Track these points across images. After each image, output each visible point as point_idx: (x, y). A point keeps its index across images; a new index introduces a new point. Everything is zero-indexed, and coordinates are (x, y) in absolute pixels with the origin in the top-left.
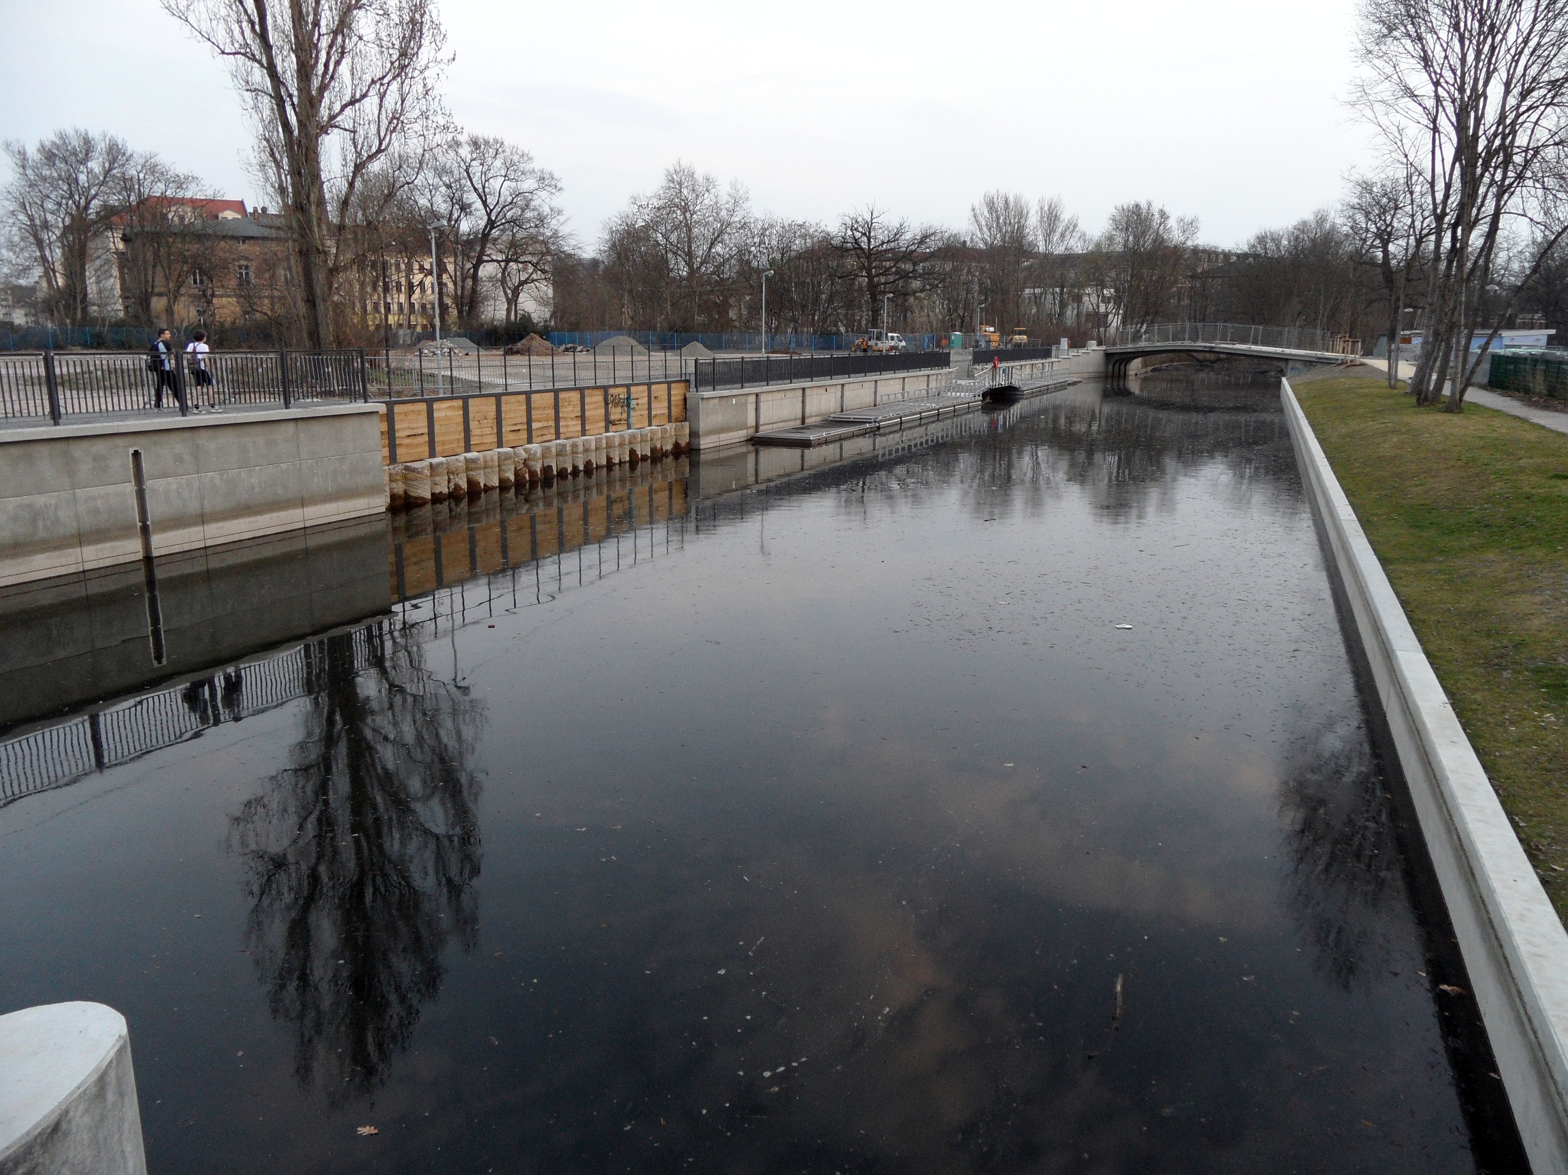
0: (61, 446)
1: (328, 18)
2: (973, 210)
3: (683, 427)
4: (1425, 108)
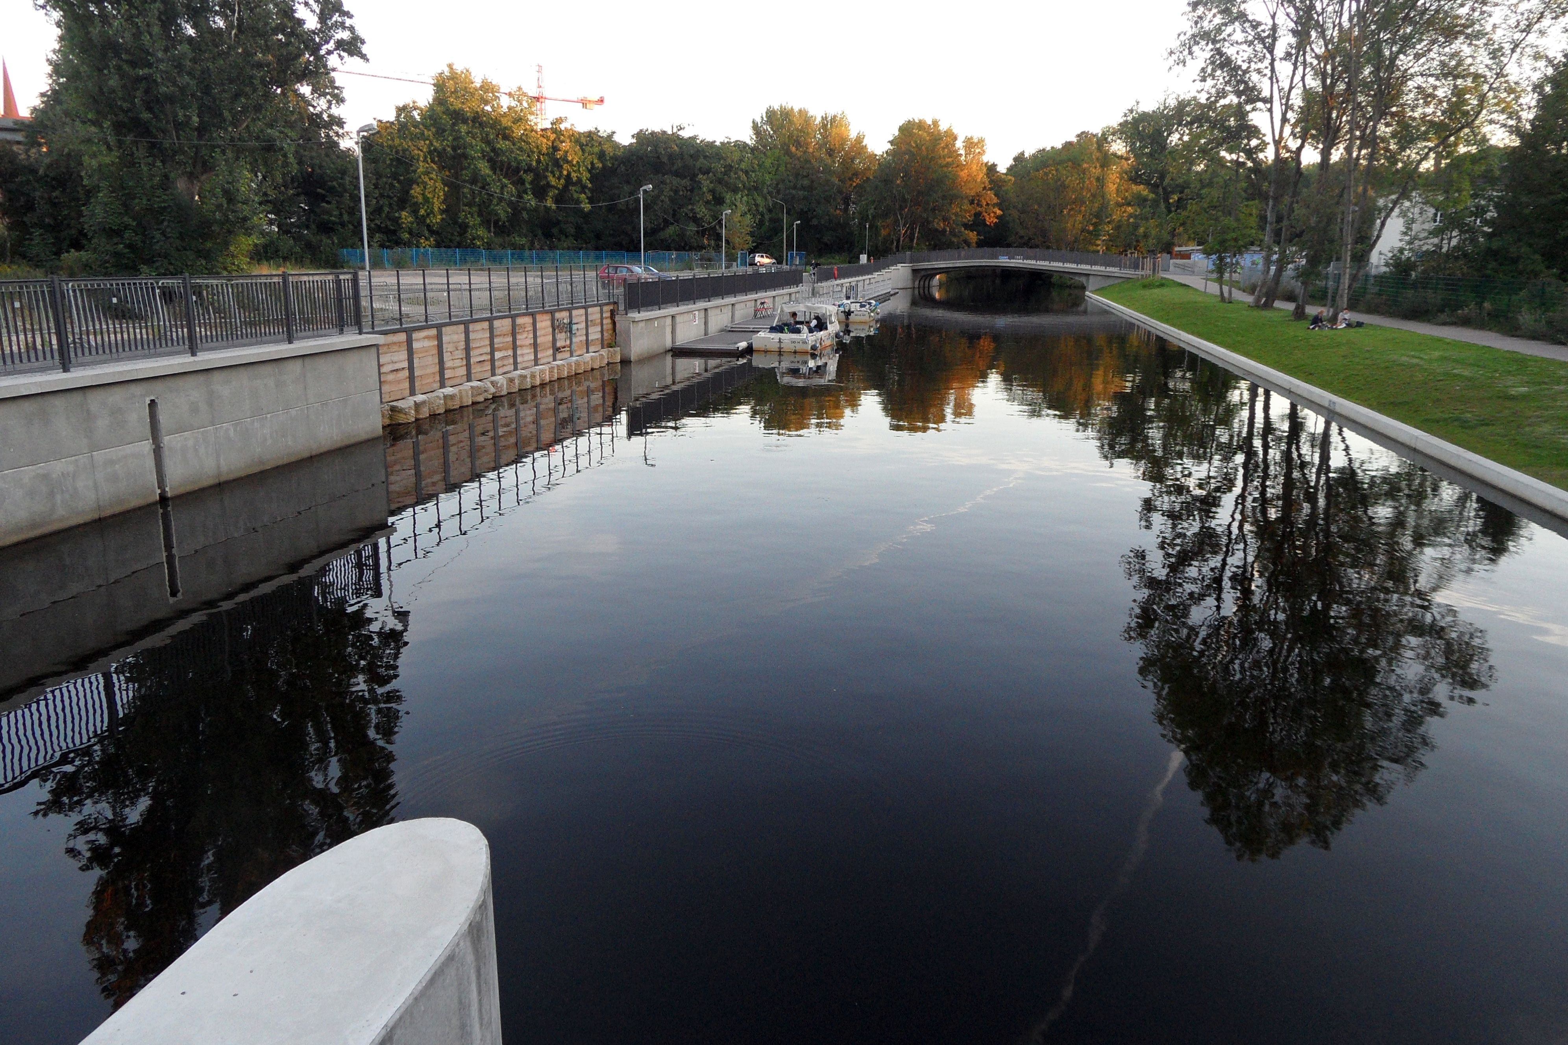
0: (77, 397)
3: (615, 352)
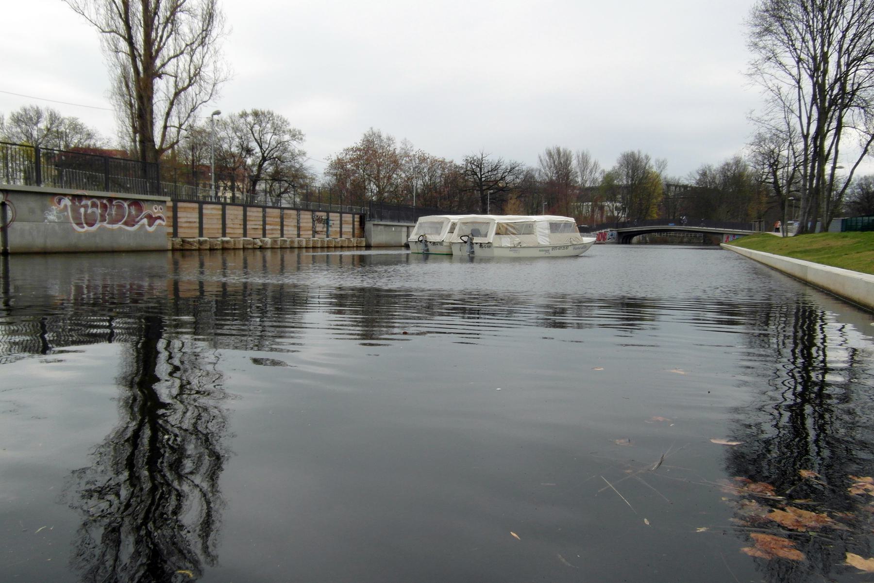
1: (163, 12)
2: (540, 157)
4: (793, 76)
